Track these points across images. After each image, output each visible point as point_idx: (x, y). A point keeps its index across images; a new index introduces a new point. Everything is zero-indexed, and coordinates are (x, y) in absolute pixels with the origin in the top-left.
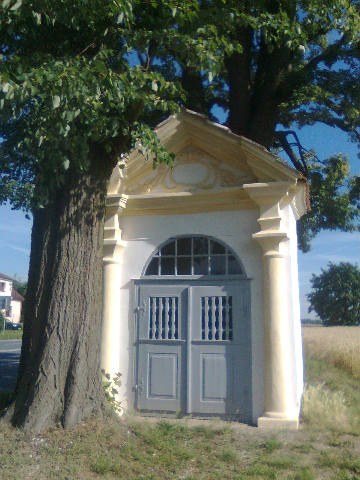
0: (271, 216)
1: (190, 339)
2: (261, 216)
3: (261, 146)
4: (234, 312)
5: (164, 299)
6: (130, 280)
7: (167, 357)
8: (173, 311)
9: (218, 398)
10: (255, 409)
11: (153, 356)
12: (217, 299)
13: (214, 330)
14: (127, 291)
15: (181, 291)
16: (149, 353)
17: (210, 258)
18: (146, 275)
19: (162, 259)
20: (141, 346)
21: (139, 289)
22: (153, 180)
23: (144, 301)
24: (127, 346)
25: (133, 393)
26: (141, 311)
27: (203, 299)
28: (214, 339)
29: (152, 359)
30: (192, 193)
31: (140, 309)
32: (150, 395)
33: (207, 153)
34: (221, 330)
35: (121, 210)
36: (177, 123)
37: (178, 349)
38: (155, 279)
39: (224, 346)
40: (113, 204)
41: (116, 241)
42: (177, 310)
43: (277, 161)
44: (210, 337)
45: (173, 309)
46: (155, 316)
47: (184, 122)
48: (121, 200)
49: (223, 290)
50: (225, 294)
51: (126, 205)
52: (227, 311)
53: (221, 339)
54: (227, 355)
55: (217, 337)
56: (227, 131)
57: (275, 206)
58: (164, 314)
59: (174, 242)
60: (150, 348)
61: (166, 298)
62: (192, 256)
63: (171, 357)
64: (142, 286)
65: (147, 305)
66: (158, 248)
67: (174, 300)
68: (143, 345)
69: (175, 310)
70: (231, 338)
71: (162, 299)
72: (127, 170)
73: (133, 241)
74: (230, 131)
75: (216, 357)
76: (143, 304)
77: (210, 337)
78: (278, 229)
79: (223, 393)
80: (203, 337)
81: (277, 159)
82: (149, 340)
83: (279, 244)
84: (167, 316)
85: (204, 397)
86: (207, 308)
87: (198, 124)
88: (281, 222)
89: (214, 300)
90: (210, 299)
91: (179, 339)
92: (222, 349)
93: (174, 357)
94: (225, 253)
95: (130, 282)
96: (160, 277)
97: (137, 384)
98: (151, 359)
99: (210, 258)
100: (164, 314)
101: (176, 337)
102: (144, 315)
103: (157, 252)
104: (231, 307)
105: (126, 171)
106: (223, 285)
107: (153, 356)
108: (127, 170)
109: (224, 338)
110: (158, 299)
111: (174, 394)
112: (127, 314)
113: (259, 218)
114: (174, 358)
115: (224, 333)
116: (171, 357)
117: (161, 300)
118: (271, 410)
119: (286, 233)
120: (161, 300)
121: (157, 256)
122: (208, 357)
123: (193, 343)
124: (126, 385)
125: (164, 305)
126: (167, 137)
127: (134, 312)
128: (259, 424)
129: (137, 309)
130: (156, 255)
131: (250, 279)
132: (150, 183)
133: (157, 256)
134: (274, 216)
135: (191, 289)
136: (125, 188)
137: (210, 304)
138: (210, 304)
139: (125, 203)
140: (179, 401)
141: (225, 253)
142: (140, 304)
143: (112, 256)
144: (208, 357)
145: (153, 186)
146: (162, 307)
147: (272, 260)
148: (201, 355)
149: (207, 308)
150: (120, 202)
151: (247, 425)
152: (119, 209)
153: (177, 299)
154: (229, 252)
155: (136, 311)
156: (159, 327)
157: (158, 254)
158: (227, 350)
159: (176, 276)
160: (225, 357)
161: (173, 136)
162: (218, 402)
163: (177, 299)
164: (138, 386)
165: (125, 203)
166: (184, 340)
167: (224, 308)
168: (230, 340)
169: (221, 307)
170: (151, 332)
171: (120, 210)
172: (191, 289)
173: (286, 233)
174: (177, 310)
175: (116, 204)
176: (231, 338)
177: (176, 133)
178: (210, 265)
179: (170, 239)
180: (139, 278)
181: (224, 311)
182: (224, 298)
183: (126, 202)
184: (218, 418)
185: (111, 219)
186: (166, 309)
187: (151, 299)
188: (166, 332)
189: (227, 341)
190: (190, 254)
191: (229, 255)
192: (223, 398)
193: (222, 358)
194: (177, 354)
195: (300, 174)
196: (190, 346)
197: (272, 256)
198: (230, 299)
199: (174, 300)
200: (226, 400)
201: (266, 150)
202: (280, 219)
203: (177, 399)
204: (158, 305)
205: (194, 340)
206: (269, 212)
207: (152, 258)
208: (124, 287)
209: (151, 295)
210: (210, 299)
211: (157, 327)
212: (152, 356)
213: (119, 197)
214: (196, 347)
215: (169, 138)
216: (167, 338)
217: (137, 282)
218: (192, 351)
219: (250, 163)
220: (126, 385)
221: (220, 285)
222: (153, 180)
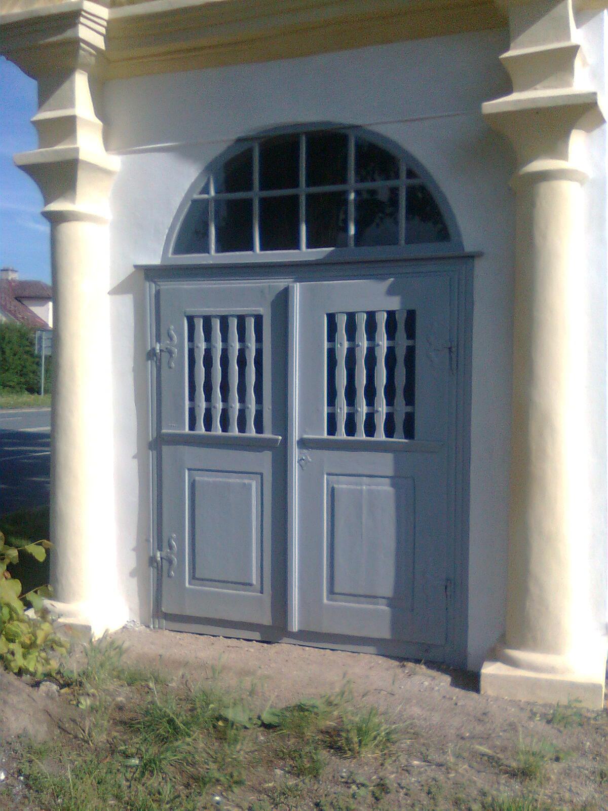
0: (545, 41)
1: (296, 434)
2: (512, 45)
4: (418, 352)
5: (224, 320)
6: (133, 270)
7: (234, 480)
8: (250, 355)
9: (372, 598)
10: (475, 640)
11: (199, 478)
12: (371, 316)
13: (363, 409)
14: (128, 301)
15: (270, 297)
16: (189, 470)
17: (352, 196)
18: (178, 250)
20: (166, 449)
21: (158, 293)
23: (172, 327)
24: (132, 448)
25: (152, 572)
26: (165, 356)
27: (331, 318)
28: (361, 436)
29: (197, 485)
31: (161, 351)
32: (193, 577)
34: (382, 408)
35: (91, 54)
37: (264, 461)
38: (198, 263)
39: (389, 457)
41: (77, 150)
42: (259, 353)
44: (351, 429)
45: (250, 351)
46: (203, 369)
49: (391, 292)
50: (394, 303)
51: (108, 38)
52: (401, 354)
53: (380, 435)
54: (396, 480)
55: (370, 429)
57: (560, 6)
58: (242, 362)
60: (191, 455)
61: (247, 319)
62: (303, 190)
63: (246, 481)
64: (167, 286)
65: (181, 335)
66: (209, 169)
67: (251, 324)
68: (172, 448)
69: (253, 354)
70: (409, 432)
71: (253, 320)
73: (135, 152)
75: (365, 486)
76: (171, 338)
77: (351, 429)
78: (569, 84)
79: (386, 586)
80: (332, 429)
82: (188, 435)
83: (566, 135)
84: (235, 368)
85: (331, 591)
86: (343, 346)
88: (578, 62)
89: (362, 321)
90: (351, 317)
91: (267, 435)
92: (385, 463)
93: (254, 484)
95: (130, 277)
96: (213, 256)
97: (160, 548)
98: (193, 485)
99: (352, 196)
100: (242, 362)
101: (259, 428)
102: (173, 365)
103: (202, 185)
104: (410, 343)
106: (390, 275)
107: (199, 478)
109: (389, 432)
110: (207, 321)
111: (255, 580)
112: (130, 363)
113: (507, 49)
114: (254, 485)
115: (390, 417)
116: (246, 481)
117: (217, 325)
118: (521, 644)
119: (595, 94)
120: (217, 325)
121: (206, 196)
122: (343, 485)
123: (303, 443)
124: (134, 550)
125: (225, 339)
127: (148, 359)
128: (484, 683)
129: (154, 349)
130: (201, 193)
131: (471, 257)
133: (206, 196)
134: (558, 40)
135: (297, 290)
137: (351, 336)
138: (351, 336)
140: (267, 598)
142: (162, 338)
143: (73, 200)
144: (343, 485)
146: (221, 343)
147: (544, 187)
148: (325, 476)
149: (343, 346)
151: (447, 679)
152: (81, 52)
153: (259, 319)
154: (411, 174)
155: (151, 354)
156: (230, 400)
157: (206, 190)
158: (397, 462)
159: (258, 255)
160: (393, 485)
162: (371, 606)
163: (259, 319)
164: (164, 554)
166: (280, 438)
167: (391, 343)
168: (406, 438)
169: (383, 343)
170: (192, 411)
171: (84, 53)
172: (297, 290)
173: (595, 94)
174: (259, 353)
175: (68, 34)
176: (409, 432)
179: (239, 140)
180: (156, 261)
181: (391, 351)
182: (391, 314)
183: (103, 31)
184: (372, 649)
185: (66, 86)
186: (230, 350)
187: (191, 320)
188: (230, 413)
189: (399, 439)
190: (296, 185)
191: (411, 182)
192: (384, 598)
193: (385, 488)
194: (262, 474)
196: (296, 453)
197: (545, 176)
198: (411, 316)
199: (251, 324)
200: (392, 602)
202: (574, 49)
203: (262, 593)
204: (208, 338)
205: (305, 436)
206: (537, 28)
207: (190, 202)
208: (118, 290)
209: (191, 311)
210: (351, 317)
211: (208, 399)
212: (197, 478)
214: (308, 455)
216: (235, 431)
217: (150, 273)
218: (301, 465)
220: (134, 550)
221: (382, 277)
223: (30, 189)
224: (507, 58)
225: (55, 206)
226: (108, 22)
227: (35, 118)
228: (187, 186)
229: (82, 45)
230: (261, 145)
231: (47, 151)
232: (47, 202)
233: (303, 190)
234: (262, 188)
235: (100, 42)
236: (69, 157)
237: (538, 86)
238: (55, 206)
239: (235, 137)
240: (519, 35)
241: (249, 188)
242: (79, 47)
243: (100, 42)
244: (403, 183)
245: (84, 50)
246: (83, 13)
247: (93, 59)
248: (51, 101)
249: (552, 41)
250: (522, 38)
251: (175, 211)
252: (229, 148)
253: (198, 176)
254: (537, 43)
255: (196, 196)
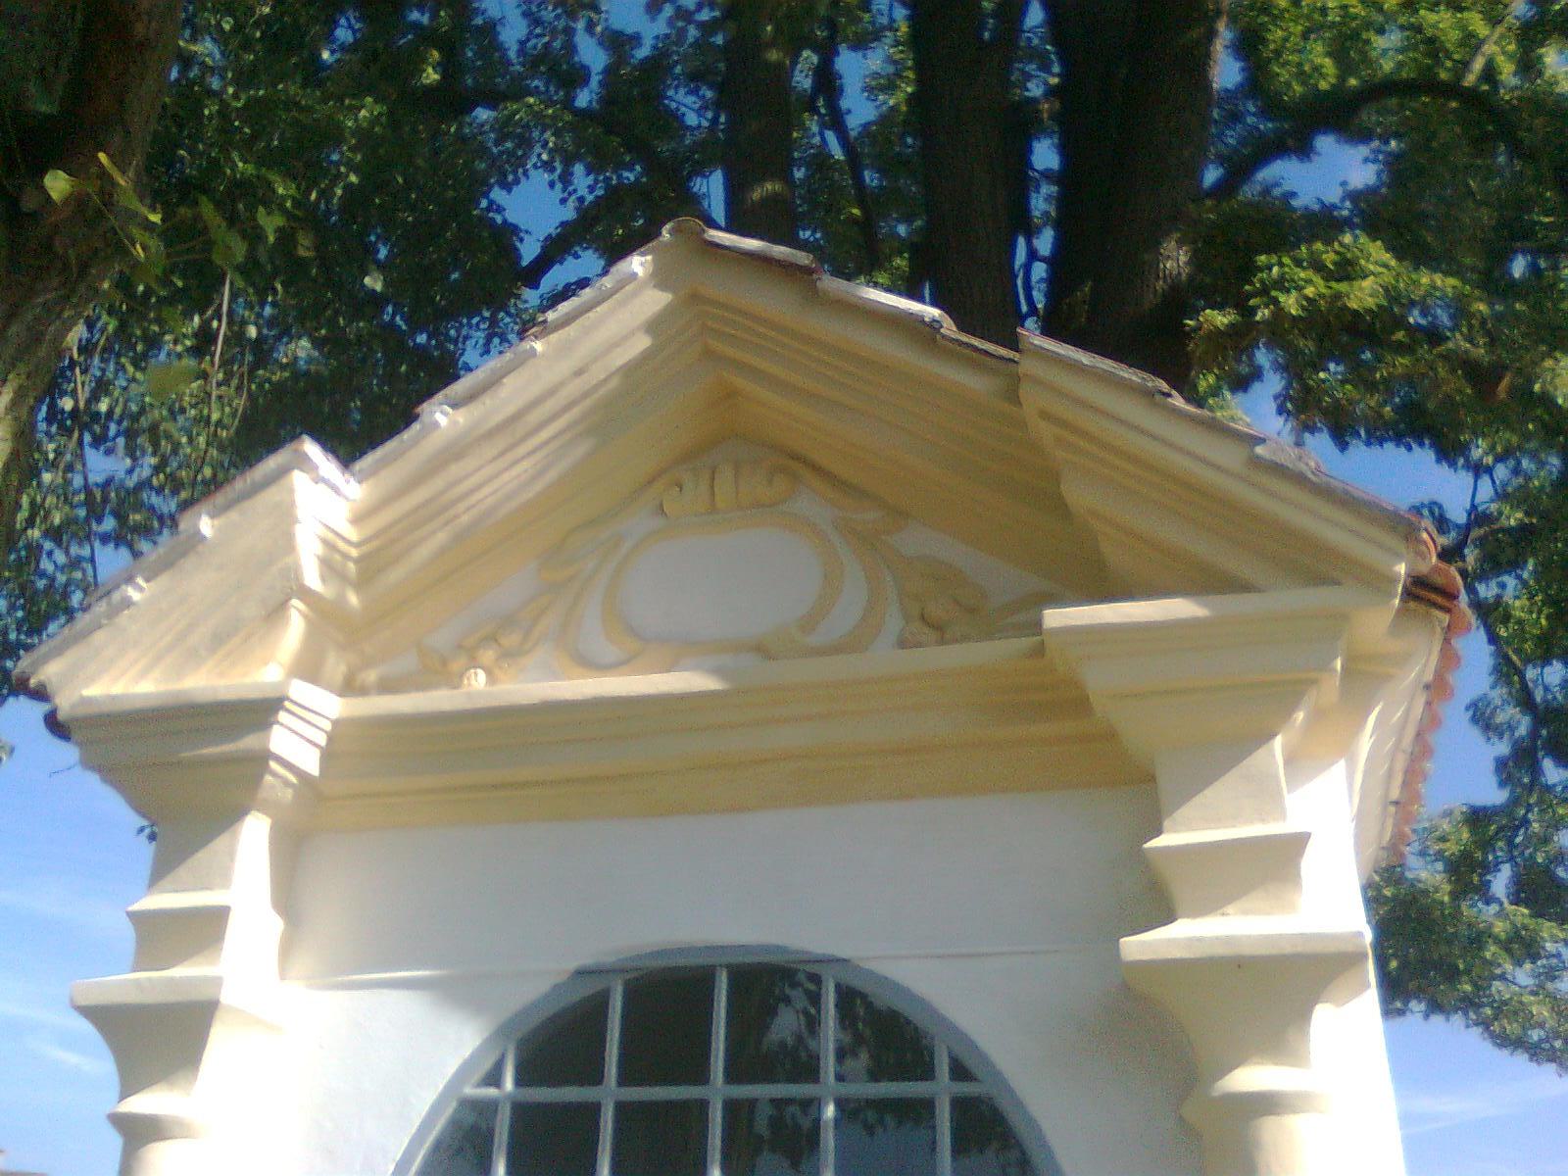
0: (1235, 819)
2: (1166, 824)
3: (1146, 375)
17: (830, 1111)
19: (523, 1113)
22: (508, 621)
30: (718, 672)
33: (817, 469)
35: (287, 783)
36: (656, 300)
40: (233, 740)
43: (1257, 462)
47: (695, 298)
48: (282, 716)
51: (328, 755)
56: (934, 326)
57: (1260, 754)
59: (598, 1003)
62: (717, 1090)
66: (502, 1032)
72: (357, 561)
74: (949, 327)
81: (1259, 450)
83: (1303, 1016)
87: (774, 302)
94: (927, 1073)
103: (487, 1064)
105: (351, 566)
108: (357, 561)
113: (1158, 832)
121: (492, 1092)
126: (597, 373)
132: (492, 639)
133: (492, 1092)
136: (342, 669)
139: (316, 745)
141: (927, 1073)
145: (508, 655)
150: (276, 728)
152: (268, 778)
157: (494, 1078)
161: (630, 369)
165: (316, 745)
171: (276, 784)
175: (249, 742)
177: (646, 357)
178: (718, 1156)
179: (581, 973)
183: (322, 740)
185: (220, 843)
190: (701, 1077)
195: (1425, 536)
197: (1267, 1104)
201: (1178, 401)
206: (1214, 795)
207: (454, 1104)
213: (278, 695)
215: (605, 380)
219: (1079, 495)
222: (508, 621)
223: (97, 1063)
224: (1151, 849)
225: (144, 1103)
226: (336, 723)
227: (136, 907)
228: (452, 1066)
229: (273, 765)
230: (627, 985)
231: (149, 979)
232: (126, 1092)
233: (717, 1090)
234: (624, 1080)
235: (311, 763)
236: (203, 994)
237: (1230, 909)
238: (144, 1103)
239: (573, 965)
240: (1179, 806)
241: (597, 1079)
242: (266, 769)
243: (311, 763)
244: (942, 1089)
245: (275, 774)
246: (287, 704)
247: (289, 794)
248: (182, 872)
249: (1249, 821)
250: (1185, 812)
251: (417, 1122)
252: (556, 987)
253: (481, 1046)
254: (1217, 822)
255: (470, 1091)
